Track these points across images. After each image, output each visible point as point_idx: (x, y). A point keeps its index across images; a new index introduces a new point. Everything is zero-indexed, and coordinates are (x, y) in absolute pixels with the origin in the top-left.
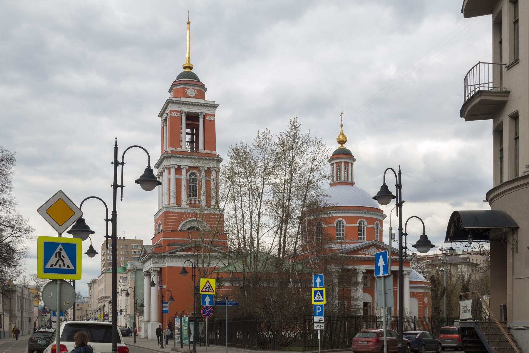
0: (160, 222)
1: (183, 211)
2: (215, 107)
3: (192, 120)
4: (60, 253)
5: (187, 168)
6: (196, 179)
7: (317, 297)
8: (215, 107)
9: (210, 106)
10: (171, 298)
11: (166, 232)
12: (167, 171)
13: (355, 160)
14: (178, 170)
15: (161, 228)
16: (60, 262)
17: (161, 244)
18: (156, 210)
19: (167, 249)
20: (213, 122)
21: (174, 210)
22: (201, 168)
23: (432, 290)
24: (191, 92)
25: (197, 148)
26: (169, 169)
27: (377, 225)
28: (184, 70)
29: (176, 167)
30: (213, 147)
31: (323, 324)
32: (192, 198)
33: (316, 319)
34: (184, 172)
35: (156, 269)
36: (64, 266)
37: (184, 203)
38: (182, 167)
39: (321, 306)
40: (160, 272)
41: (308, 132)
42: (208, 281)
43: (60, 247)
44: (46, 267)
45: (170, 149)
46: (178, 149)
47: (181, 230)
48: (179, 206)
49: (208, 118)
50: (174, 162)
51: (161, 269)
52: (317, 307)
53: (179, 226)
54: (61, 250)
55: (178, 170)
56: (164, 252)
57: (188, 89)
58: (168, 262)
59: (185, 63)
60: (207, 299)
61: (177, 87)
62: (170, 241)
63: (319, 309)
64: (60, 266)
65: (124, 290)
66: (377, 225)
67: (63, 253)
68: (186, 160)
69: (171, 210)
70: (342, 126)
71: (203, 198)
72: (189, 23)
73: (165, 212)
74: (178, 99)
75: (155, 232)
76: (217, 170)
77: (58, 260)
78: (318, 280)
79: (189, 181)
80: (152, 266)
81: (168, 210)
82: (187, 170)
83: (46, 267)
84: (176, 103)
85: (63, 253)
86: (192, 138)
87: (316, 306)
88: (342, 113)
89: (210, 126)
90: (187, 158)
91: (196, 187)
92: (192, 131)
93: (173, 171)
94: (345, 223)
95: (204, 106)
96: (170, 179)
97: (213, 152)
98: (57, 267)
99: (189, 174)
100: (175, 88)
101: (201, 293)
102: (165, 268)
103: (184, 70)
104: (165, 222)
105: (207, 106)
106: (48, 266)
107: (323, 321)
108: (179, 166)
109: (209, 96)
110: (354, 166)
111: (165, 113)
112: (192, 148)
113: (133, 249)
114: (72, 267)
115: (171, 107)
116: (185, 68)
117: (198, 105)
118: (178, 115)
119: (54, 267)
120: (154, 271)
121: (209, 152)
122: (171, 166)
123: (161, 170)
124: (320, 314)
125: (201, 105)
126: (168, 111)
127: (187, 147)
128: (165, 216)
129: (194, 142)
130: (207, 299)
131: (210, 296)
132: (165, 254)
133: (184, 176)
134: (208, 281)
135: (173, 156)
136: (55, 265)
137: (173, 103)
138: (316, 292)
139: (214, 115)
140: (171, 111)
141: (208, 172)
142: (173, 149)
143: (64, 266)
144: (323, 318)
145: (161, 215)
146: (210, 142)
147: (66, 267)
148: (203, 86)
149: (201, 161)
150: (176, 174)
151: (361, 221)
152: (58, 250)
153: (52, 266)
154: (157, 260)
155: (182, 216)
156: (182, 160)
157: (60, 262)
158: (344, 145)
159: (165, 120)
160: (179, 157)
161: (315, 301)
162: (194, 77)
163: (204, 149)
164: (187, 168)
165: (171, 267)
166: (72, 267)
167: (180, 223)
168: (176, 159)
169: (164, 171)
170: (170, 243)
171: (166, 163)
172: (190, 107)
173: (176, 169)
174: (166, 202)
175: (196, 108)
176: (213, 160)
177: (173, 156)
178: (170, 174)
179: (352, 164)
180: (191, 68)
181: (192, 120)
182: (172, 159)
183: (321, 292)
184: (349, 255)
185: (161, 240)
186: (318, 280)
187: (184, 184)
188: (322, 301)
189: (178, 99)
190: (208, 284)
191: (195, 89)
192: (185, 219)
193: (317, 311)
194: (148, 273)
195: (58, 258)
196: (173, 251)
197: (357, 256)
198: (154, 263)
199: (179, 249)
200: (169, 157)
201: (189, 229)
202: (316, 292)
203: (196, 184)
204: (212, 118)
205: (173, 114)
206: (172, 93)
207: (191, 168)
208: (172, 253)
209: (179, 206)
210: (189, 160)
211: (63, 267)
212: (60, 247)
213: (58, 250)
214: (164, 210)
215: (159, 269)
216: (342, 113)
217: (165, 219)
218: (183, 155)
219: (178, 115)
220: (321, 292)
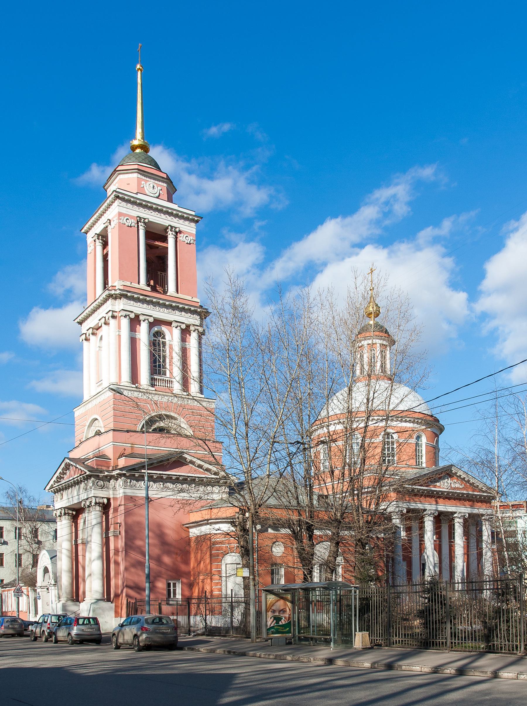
14: (135, 322)
35: (101, 501)
55: (135, 322)
71: (177, 373)
76: (201, 330)
82: (151, 325)
133: (143, 333)
140: (120, 214)
171: (109, 305)
173: (131, 319)
215: (105, 501)
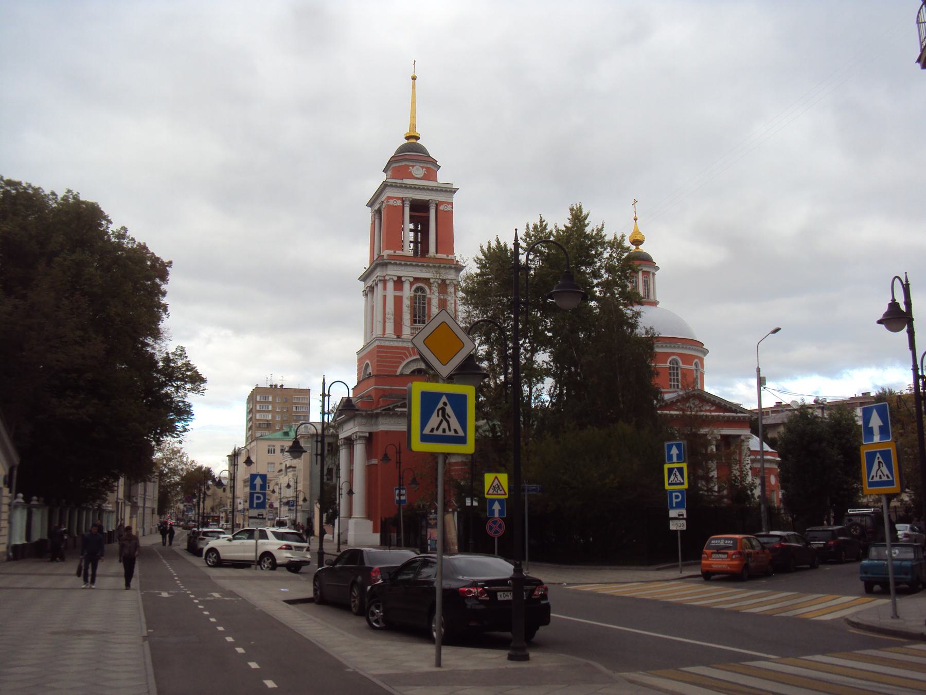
0: (368, 361)
1: (405, 345)
2: (453, 191)
3: (419, 210)
4: (443, 409)
5: (412, 280)
6: (424, 297)
7: (672, 477)
8: (453, 191)
9: (446, 191)
10: (414, 481)
11: (379, 377)
12: (380, 285)
13: (657, 268)
14: (399, 283)
15: (370, 370)
16: (444, 425)
17: (369, 396)
18: (360, 344)
19: (381, 403)
20: (450, 214)
21: (392, 344)
22: (432, 281)
23: (780, 464)
24: (418, 171)
25: (425, 250)
26: (385, 282)
27: (696, 364)
28: (406, 141)
29: (395, 279)
30: (451, 251)
31: (684, 522)
32: (417, 325)
33: (673, 513)
34: (407, 286)
36: (450, 430)
37: (407, 331)
38: (403, 279)
39: (681, 492)
40: (370, 440)
41: (600, 227)
42: (496, 478)
43: (444, 399)
44: (424, 432)
45: (386, 253)
46: (399, 253)
47: (402, 375)
48: (399, 337)
49: (441, 208)
50: (393, 272)
51: (370, 434)
52: (674, 494)
53: (398, 367)
54: (445, 404)
55: (399, 283)
56: (377, 409)
57: (413, 166)
58: (383, 424)
59: (406, 130)
60: (497, 507)
61: (397, 165)
62: (384, 390)
63: (677, 497)
64: (444, 431)
65: (290, 467)
66: (696, 364)
67: (449, 410)
68: (418, 269)
69: (387, 344)
70: (636, 219)
72: (414, 78)
73: (378, 347)
74: (400, 181)
75: (358, 378)
77: (442, 421)
78: (674, 451)
79: (414, 299)
80: (356, 429)
81: (383, 343)
82: (412, 284)
83: (424, 432)
84: (396, 186)
85: (449, 410)
86: (416, 237)
87: (671, 492)
88: (636, 202)
89: (445, 220)
90: (411, 265)
91: (424, 308)
92: (416, 226)
93: (390, 285)
94: (681, 364)
95: (437, 190)
96: (385, 297)
97: (450, 257)
98: (440, 432)
99: (414, 287)
100: (394, 165)
101: (487, 496)
102: (377, 433)
103: (406, 141)
104: (378, 361)
105: (441, 191)
106: (427, 431)
107: (685, 516)
108: (399, 278)
109: (443, 177)
110: (656, 277)
111: (379, 201)
112: (415, 250)
113: (295, 404)
114: (461, 433)
115: (389, 193)
116: (407, 138)
117: (428, 189)
118: (399, 203)
119: (435, 432)
120: (360, 437)
121: (444, 256)
122: (387, 278)
123: (369, 284)
124: (679, 505)
125: (432, 190)
126: (383, 198)
127: (409, 249)
128: (378, 352)
129: (422, 243)
130: (497, 507)
131: (500, 501)
132: (378, 411)
133: (407, 292)
134: (496, 478)
135: (390, 263)
136: (437, 429)
137: (391, 186)
138: (670, 471)
139: (451, 204)
140: (389, 198)
141: (443, 286)
142: (391, 252)
143: (450, 430)
144: (684, 512)
145: (370, 353)
146: (446, 241)
147: (452, 433)
148: (434, 162)
149: (442, 271)
150: (395, 289)
151: (674, 360)
152: (440, 405)
153: (432, 430)
154: (364, 421)
155: (401, 353)
156: (403, 268)
157: (444, 425)
158: (640, 247)
159: (379, 212)
160: (400, 264)
161: (669, 484)
162: (421, 150)
163: (437, 252)
164: (412, 280)
165: (387, 432)
166: (461, 433)
167: (401, 363)
168: (395, 267)
169: (377, 285)
170: (384, 394)
171: (379, 273)
172: (417, 192)
174: (378, 332)
175: (424, 193)
176: (450, 268)
177: (390, 263)
178: (385, 288)
179: (654, 274)
180: (417, 138)
181: (419, 210)
182: (390, 267)
183: (680, 470)
184: (713, 414)
185: (371, 387)
186: (674, 451)
187: (406, 302)
188: (683, 484)
189: (400, 181)
190: (496, 482)
191: (423, 168)
192: (407, 357)
193: (674, 500)
194: (349, 442)
195: (441, 417)
196: (391, 407)
197: (672, 412)
198: (360, 425)
199: (399, 404)
200: (384, 265)
201: (413, 372)
202: (670, 471)
203: (424, 304)
204: (449, 208)
205: (391, 202)
206: (389, 173)
207: (417, 280)
208: (389, 409)
209: (399, 337)
210: (424, 270)
211: (448, 433)
212: (444, 399)
213: (440, 405)
214: (377, 343)
215: (367, 435)
216: (636, 202)
217: (378, 356)
218: (403, 261)
219: (399, 203)
220: (680, 470)
